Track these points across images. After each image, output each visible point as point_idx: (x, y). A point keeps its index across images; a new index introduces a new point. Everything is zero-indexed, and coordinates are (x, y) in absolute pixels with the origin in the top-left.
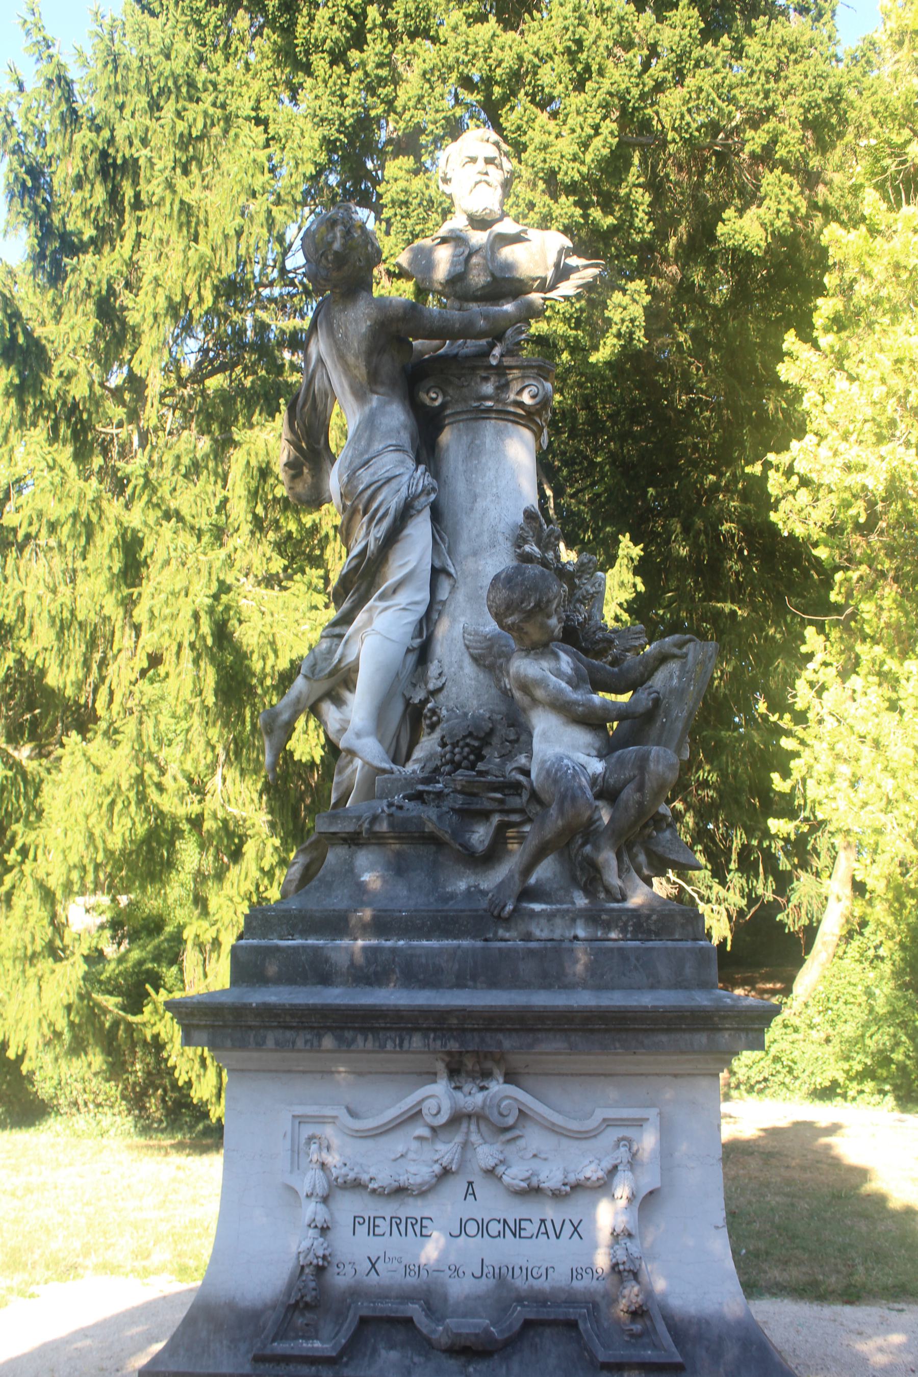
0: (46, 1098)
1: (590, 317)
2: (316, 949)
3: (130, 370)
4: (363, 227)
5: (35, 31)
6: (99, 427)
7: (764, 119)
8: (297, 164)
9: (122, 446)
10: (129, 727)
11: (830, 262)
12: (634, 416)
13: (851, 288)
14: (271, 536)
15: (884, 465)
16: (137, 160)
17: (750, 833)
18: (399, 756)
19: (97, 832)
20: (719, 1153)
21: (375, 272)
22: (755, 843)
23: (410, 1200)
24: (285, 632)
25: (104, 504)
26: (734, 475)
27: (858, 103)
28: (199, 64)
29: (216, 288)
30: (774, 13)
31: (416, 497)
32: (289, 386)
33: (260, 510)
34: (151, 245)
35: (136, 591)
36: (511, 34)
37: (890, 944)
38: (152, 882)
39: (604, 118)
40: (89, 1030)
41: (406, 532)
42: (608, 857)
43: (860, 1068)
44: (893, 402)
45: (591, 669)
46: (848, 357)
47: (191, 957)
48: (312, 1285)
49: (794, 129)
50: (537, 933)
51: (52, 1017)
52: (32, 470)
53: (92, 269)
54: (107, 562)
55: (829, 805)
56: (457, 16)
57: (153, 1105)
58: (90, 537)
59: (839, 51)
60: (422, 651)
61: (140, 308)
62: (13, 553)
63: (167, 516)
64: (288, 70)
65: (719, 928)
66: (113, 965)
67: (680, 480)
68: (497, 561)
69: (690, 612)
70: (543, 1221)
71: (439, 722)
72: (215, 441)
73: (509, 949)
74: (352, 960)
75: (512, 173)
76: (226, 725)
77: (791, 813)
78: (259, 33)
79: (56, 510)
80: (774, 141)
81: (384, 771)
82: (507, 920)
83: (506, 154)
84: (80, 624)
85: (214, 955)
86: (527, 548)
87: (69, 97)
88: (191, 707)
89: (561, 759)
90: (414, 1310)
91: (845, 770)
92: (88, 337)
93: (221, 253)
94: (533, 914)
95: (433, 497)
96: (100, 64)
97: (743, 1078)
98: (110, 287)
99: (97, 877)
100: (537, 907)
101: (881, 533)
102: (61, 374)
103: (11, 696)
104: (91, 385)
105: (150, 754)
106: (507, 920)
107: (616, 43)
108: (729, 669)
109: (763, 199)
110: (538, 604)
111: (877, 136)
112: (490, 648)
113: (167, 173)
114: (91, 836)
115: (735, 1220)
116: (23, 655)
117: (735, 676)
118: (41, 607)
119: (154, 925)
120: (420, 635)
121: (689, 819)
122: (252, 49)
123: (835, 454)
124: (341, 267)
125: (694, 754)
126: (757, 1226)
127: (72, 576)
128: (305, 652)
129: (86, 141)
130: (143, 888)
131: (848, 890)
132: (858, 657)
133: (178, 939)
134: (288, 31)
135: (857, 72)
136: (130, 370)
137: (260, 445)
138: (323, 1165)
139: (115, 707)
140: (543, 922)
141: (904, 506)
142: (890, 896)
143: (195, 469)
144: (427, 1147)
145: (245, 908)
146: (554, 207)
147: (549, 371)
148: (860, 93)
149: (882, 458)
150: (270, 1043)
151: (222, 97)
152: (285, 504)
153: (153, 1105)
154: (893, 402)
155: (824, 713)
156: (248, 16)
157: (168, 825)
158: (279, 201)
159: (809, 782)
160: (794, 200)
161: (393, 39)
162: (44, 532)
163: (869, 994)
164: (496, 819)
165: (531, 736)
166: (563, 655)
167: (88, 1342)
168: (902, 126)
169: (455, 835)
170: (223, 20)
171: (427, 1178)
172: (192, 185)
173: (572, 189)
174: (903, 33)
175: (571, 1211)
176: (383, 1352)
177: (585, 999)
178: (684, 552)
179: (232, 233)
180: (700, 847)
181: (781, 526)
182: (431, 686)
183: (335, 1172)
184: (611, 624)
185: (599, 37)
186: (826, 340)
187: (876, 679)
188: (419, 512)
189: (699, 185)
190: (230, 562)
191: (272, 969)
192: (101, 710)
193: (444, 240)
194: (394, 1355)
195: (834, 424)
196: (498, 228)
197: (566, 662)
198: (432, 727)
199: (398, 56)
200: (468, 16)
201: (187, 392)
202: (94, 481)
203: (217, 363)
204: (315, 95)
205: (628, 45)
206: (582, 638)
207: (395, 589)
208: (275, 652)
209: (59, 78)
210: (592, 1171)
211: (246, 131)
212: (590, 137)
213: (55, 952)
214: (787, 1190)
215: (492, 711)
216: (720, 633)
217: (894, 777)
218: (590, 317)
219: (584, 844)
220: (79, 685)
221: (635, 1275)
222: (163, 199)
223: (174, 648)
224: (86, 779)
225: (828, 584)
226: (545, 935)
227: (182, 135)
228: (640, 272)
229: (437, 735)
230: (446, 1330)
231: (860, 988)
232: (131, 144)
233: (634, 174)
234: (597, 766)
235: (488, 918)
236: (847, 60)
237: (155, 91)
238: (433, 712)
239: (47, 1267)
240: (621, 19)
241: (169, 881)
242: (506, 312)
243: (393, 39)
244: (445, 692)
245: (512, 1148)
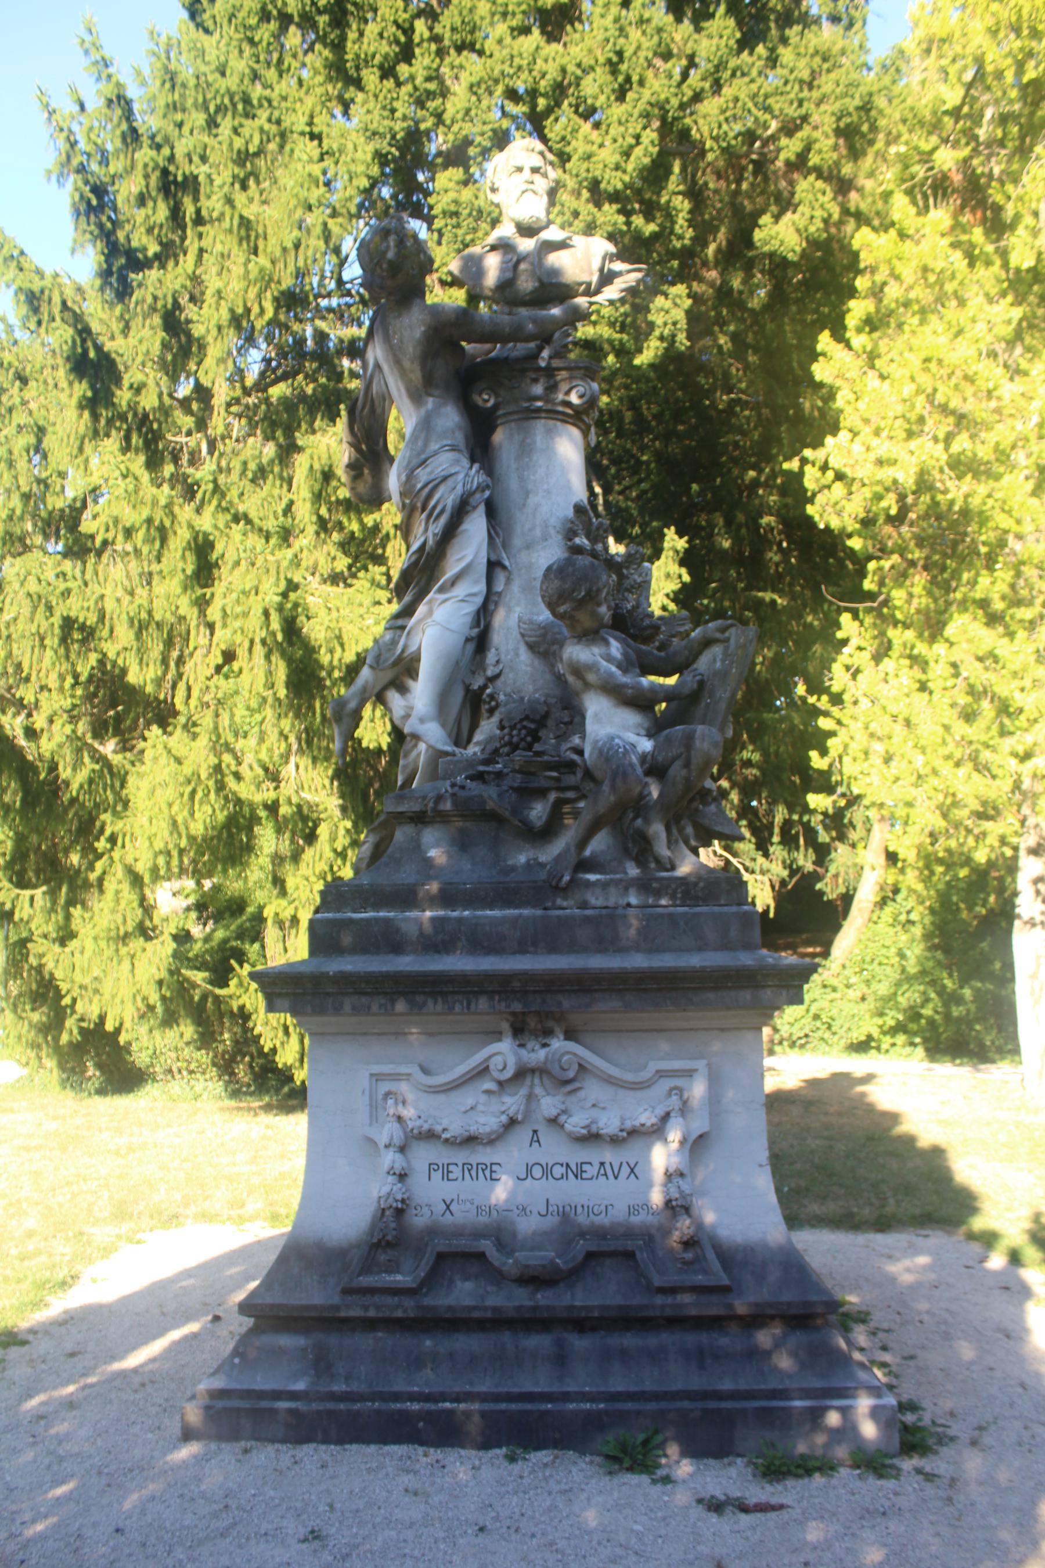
0: (142, 1066)
1: (634, 322)
2: (387, 921)
3: (197, 381)
4: (415, 236)
5: (93, 51)
6: (169, 437)
7: (798, 128)
9: (192, 454)
10: (206, 720)
11: (862, 265)
12: (678, 415)
13: (881, 290)
14: (336, 536)
15: (914, 460)
16: (196, 177)
17: (791, 810)
18: (461, 739)
19: (180, 820)
20: (763, 1100)
21: (428, 280)
22: (795, 817)
23: (480, 1148)
24: (350, 627)
25: (176, 509)
26: (773, 470)
27: (888, 111)
29: (276, 299)
30: (807, 21)
31: (471, 494)
33: (324, 511)
34: (212, 260)
35: (208, 591)
36: (555, 47)
37: (921, 908)
38: (233, 866)
39: (645, 128)
40: (178, 1003)
41: (463, 527)
42: (657, 830)
43: (892, 1023)
44: (922, 398)
45: (640, 654)
46: (879, 356)
47: (271, 933)
48: (393, 1225)
49: (827, 136)
50: (593, 901)
51: (145, 991)
52: (107, 480)
53: (156, 284)
54: (180, 565)
56: (501, 29)
57: (242, 1071)
58: (164, 540)
59: (870, 59)
60: (480, 640)
61: (205, 320)
62: (92, 559)
63: (236, 519)
64: (339, 85)
65: (762, 895)
66: (199, 944)
67: (722, 475)
68: (548, 554)
69: (732, 601)
70: (602, 1164)
71: (497, 706)
74: (421, 929)
76: (297, 716)
78: (311, 48)
79: (131, 517)
80: (808, 149)
81: (446, 754)
83: (551, 163)
84: (158, 624)
85: (293, 931)
86: (577, 541)
87: (128, 115)
88: (265, 700)
89: (612, 738)
90: (486, 1246)
91: (878, 748)
92: (156, 349)
94: (588, 884)
95: (487, 493)
96: (158, 83)
97: (786, 1035)
99: (181, 861)
100: (592, 877)
101: (911, 525)
102: (131, 387)
103: (95, 695)
104: (160, 395)
105: (227, 744)
107: (655, 54)
110: (589, 593)
111: (907, 143)
112: (544, 635)
113: (226, 189)
114: (175, 823)
115: (777, 1160)
116: (105, 655)
117: (776, 662)
118: (120, 610)
119: (237, 906)
120: (478, 625)
121: (734, 796)
122: (304, 65)
123: (868, 449)
126: (798, 1166)
127: (148, 578)
129: (147, 160)
130: (225, 871)
131: (882, 860)
132: (890, 642)
133: (259, 919)
134: (338, 47)
135: (887, 80)
136: (197, 381)
137: (323, 449)
138: (399, 1119)
139: (193, 702)
140: (598, 890)
141: (933, 498)
142: (921, 864)
143: (261, 474)
145: (320, 886)
146: (598, 215)
147: (596, 372)
148: (890, 101)
149: (912, 453)
150: (347, 1008)
151: (276, 114)
152: (347, 506)
153: (242, 1071)
155: (859, 694)
156: (299, 33)
157: (246, 810)
158: (334, 214)
159: (845, 759)
161: (441, 53)
162: (120, 538)
163: (901, 955)
164: (553, 796)
165: (584, 717)
166: (612, 641)
168: (930, 133)
169: (515, 812)
171: (495, 1127)
172: (251, 200)
174: (931, 42)
175: (628, 1154)
176: (459, 1283)
177: (638, 961)
178: (726, 544)
179: (289, 245)
180: (744, 822)
181: (817, 518)
182: (489, 673)
183: (410, 1124)
184: (658, 613)
185: (639, 48)
186: (860, 341)
187: (907, 662)
188: (475, 508)
189: (737, 192)
190: (296, 562)
191: (347, 940)
192: (179, 705)
193: (493, 248)
194: (469, 1285)
195: (866, 421)
196: (547, 235)
197: (615, 648)
198: (491, 711)
199: (445, 70)
200: (512, 29)
201: (251, 400)
202: (166, 487)
203: (279, 372)
205: (667, 56)
206: (630, 623)
208: (342, 645)
209: (119, 97)
210: (647, 1118)
212: (631, 147)
213: (145, 932)
214: (826, 1133)
215: (547, 696)
216: (761, 621)
217: (924, 753)
218: (634, 322)
219: (634, 819)
220: (159, 682)
221: (687, 1210)
222: (222, 214)
223: (247, 644)
224: (167, 770)
225: (862, 574)
226: (600, 902)
227: (239, 152)
228: (681, 277)
229: (495, 719)
230: (516, 1262)
231: (893, 950)
232: (191, 161)
233: (674, 183)
234: (646, 745)
235: (547, 888)
236: (877, 69)
237: (212, 109)
240: (660, 30)
242: (553, 316)
243: (441, 53)
244: (502, 678)
245: (573, 1098)
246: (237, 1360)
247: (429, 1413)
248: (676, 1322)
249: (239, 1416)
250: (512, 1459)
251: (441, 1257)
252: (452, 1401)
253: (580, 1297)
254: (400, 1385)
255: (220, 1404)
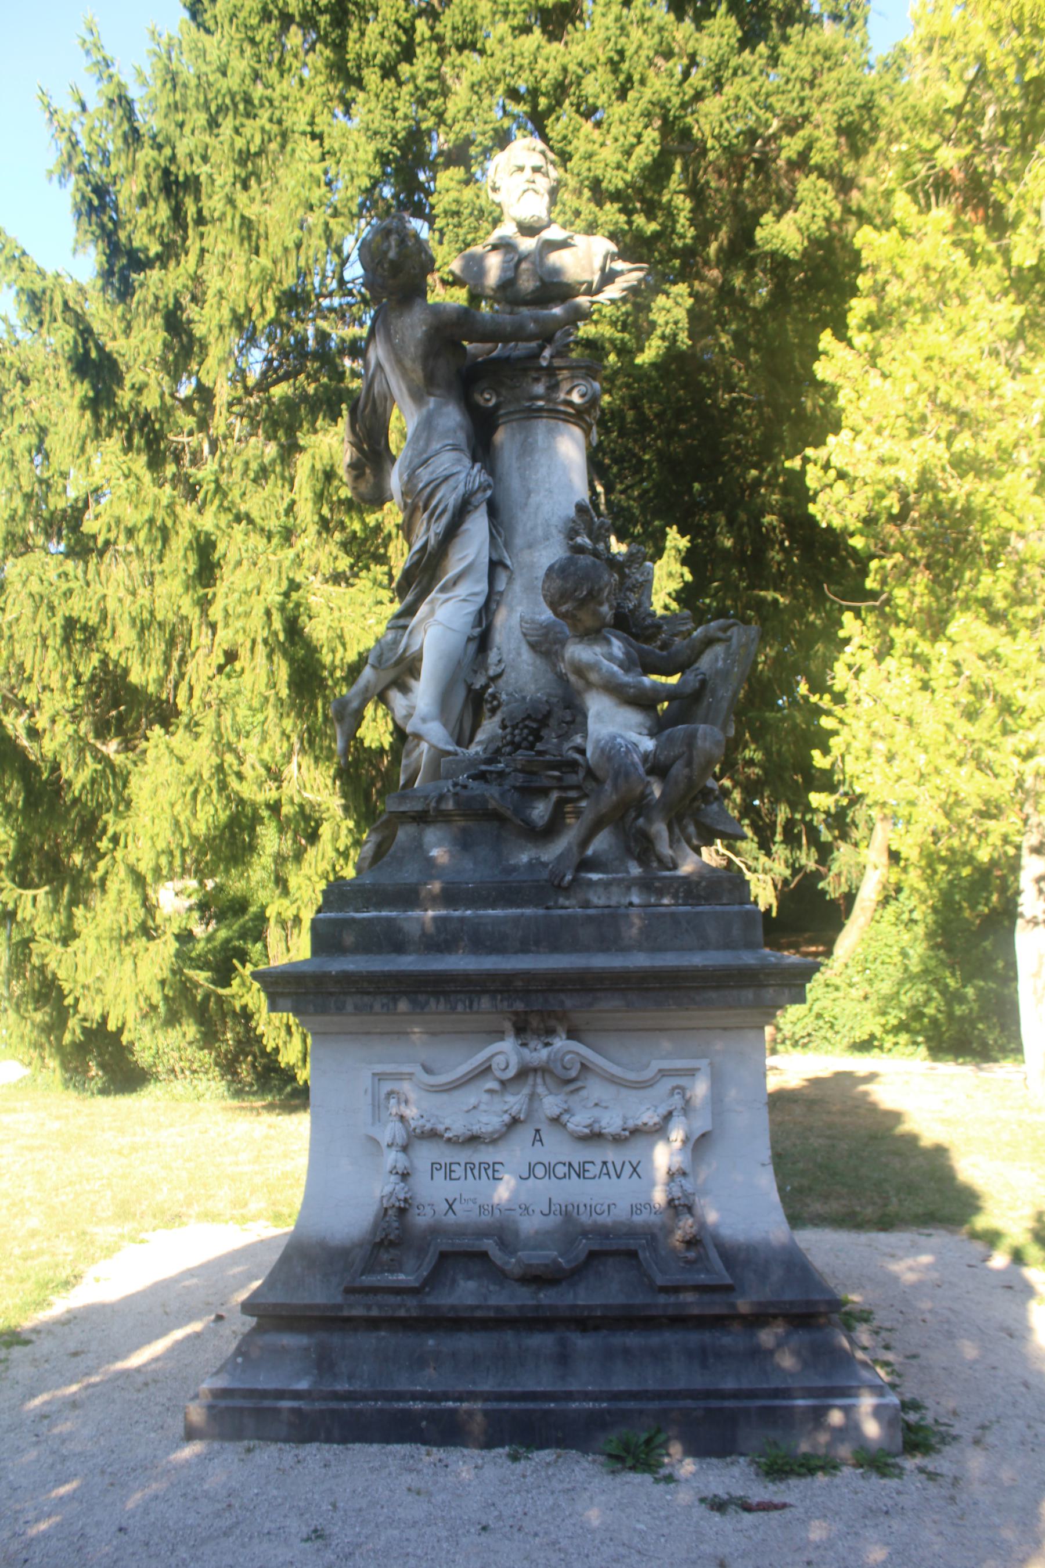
0: (145, 1066)
1: (636, 321)
2: (389, 920)
3: (199, 380)
4: (416, 236)
5: (94, 51)
7: (800, 127)
8: (352, 179)
10: (209, 720)
11: (864, 264)
12: (680, 414)
13: (883, 289)
14: (338, 536)
15: (916, 459)
16: (197, 177)
17: (793, 809)
18: (463, 739)
19: (182, 819)
20: (765, 1099)
21: (430, 279)
22: (798, 816)
23: (483, 1147)
24: (352, 627)
25: (178, 509)
26: (774, 469)
27: (889, 109)
28: (254, 81)
29: (277, 299)
30: (808, 20)
32: (350, 392)
33: (325, 511)
34: (214, 260)
35: (210, 591)
36: (556, 46)
37: (923, 907)
39: (646, 127)
40: (181, 1003)
41: (465, 527)
42: (660, 829)
43: (895, 1022)
45: (641, 653)
46: (881, 355)
47: (273, 933)
48: (396, 1224)
50: (595, 900)
51: (148, 991)
52: (108, 480)
53: (157, 284)
54: (182, 565)
55: (866, 779)
56: (503, 28)
57: (244, 1070)
58: (166, 540)
59: (872, 58)
60: (482, 640)
61: (206, 320)
62: (94, 559)
63: (238, 519)
64: (341, 85)
65: (764, 894)
66: (202, 944)
67: (724, 475)
68: (550, 553)
69: (735, 600)
70: (605, 1163)
72: (281, 446)
73: (569, 916)
75: (559, 181)
76: (299, 715)
77: (831, 788)
78: (312, 48)
79: (133, 517)
80: (809, 147)
81: (448, 753)
82: (567, 889)
83: (553, 163)
84: (160, 624)
85: (296, 931)
86: (579, 540)
87: (130, 115)
88: (267, 699)
89: (614, 738)
90: (489, 1245)
91: (881, 747)
92: (158, 349)
93: (282, 265)
94: (591, 883)
95: (489, 493)
96: (159, 83)
98: (177, 302)
99: (184, 861)
100: (595, 876)
101: (913, 524)
102: (133, 387)
103: (97, 695)
104: (162, 396)
105: (229, 744)
106: (567, 889)
107: (657, 53)
108: (772, 654)
109: (798, 204)
110: (590, 593)
111: (908, 142)
112: (546, 635)
113: (227, 189)
114: (177, 823)
115: (780, 1160)
116: (107, 655)
117: (778, 661)
119: (239, 906)
121: (737, 795)
122: (305, 64)
123: (870, 448)
124: (396, 274)
125: (739, 734)
126: (801, 1165)
128: (372, 644)
129: (148, 160)
130: (227, 871)
131: (884, 859)
132: (892, 640)
133: (261, 918)
134: (340, 47)
135: (888, 79)
136: (199, 380)
137: (325, 448)
138: (402, 1118)
139: (195, 702)
140: (600, 890)
141: (935, 497)
142: (923, 863)
143: (263, 473)
144: (496, 1099)
145: (322, 885)
147: (597, 372)
148: (892, 99)
149: (914, 451)
150: (350, 1008)
151: (277, 114)
152: (349, 505)
153: (244, 1070)
154: (923, 400)
155: (861, 693)
156: (300, 33)
157: (249, 810)
158: (336, 214)
159: (847, 758)
160: (829, 205)
161: (442, 52)
162: (122, 538)
163: (904, 954)
164: (555, 795)
165: (585, 717)
167: (195, 1281)
168: (932, 131)
170: (278, 36)
172: (252, 200)
173: (616, 196)
174: (932, 40)
175: (630, 1153)
176: (462, 1283)
177: (640, 960)
178: (728, 543)
179: (291, 245)
181: (819, 517)
184: (660, 612)
185: (640, 47)
186: (861, 339)
187: (909, 661)
188: (476, 507)
189: (739, 191)
190: (298, 561)
191: (349, 939)
192: (181, 705)
193: (495, 247)
194: (471, 1285)
195: (868, 420)
196: (546, 235)
197: (617, 647)
198: (493, 711)
199: (446, 69)
200: (514, 29)
201: (253, 400)
202: (168, 488)
203: (281, 372)
204: (367, 109)
205: (668, 55)
206: (634, 624)
207: (456, 581)
208: (344, 645)
209: (120, 97)
210: (650, 1117)
211: (302, 146)
212: (633, 146)
213: (147, 931)
216: (763, 620)
218: (636, 321)
220: (161, 682)
221: (689, 1209)
222: (224, 214)
223: (249, 644)
224: (170, 770)
225: (864, 572)
226: (602, 902)
227: (240, 152)
228: (682, 276)
229: (497, 718)
230: (519, 1261)
231: (896, 949)
232: (192, 161)
233: (676, 181)
234: (648, 744)
235: (550, 887)
236: (878, 68)
237: (213, 109)
238: (494, 696)
239: (154, 1216)
240: (661, 29)
241: (250, 864)
242: (555, 316)
243: (442, 52)
244: (504, 678)
245: (576, 1098)
246: (240, 1360)
247: (432, 1412)
248: (679, 1321)
249: (242, 1415)
250: (515, 1458)
251: (443, 1256)
252: (455, 1400)
253: (584, 1296)
254: (402, 1385)
255: (223, 1403)
